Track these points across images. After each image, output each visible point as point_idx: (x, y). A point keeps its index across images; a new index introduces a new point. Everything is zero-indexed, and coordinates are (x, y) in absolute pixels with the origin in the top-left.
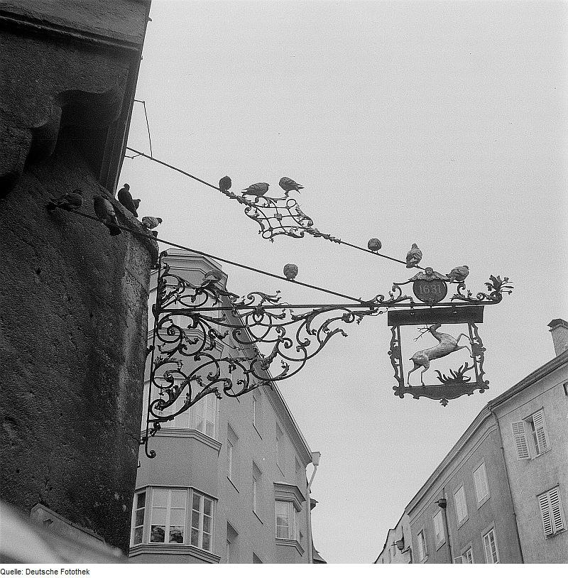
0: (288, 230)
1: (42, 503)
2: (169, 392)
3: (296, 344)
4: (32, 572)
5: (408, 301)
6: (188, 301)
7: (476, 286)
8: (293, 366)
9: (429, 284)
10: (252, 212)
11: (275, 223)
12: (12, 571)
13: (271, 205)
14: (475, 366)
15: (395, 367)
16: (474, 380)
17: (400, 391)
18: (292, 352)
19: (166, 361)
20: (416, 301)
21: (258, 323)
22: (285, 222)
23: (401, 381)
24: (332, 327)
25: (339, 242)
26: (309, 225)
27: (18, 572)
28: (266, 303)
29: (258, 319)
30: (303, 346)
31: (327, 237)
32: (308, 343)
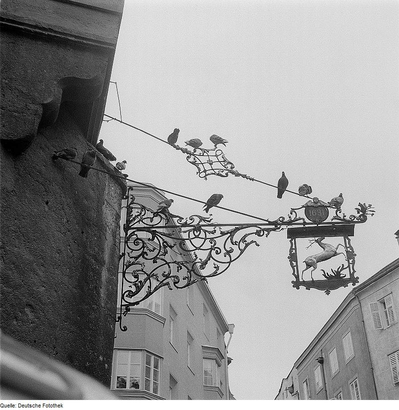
0: (217, 171)
2: (135, 285)
3: (223, 251)
4: (23, 406)
5: (301, 221)
7: (349, 210)
8: (222, 267)
9: (316, 209)
10: (191, 159)
11: (207, 166)
12: (9, 405)
13: (205, 154)
15: (293, 267)
16: (348, 276)
17: (297, 284)
20: (307, 221)
21: (197, 237)
22: (215, 166)
23: (297, 277)
24: (248, 239)
26: (232, 168)
27: (13, 406)
28: (202, 223)
29: (197, 234)
30: (228, 253)
31: (244, 176)
32: (232, 251)
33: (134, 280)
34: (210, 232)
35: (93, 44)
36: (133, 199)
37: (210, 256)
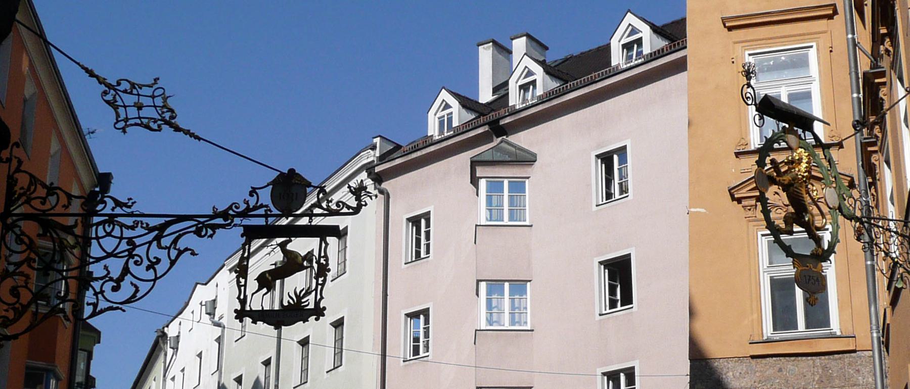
0: (145, 121)
1: (512, 39)
2: (14, 309)
3: (146, 263)
5: (261, 211)
6: (36, 203)
8: (144, 287)
11: (133, 112)
13: (135, 92)
14: (316, 289)
15: (239, 287)
16: (311, 306)
18: (139, 271)
19: (14, 273)
21: (109, 234)
22: (145, 113)
23: (243, 302)
24: (181, 244)
25: (199, 139)
26: (172, 118)
28: (118, 211)
29: (108, 229)
30: (151, 266)
31: (187, 132)
32: (158, 261)
33: (12, 300)
34: (128, 227)
35: (414, 155)
36: (20, 162)
37: (126, 271)
